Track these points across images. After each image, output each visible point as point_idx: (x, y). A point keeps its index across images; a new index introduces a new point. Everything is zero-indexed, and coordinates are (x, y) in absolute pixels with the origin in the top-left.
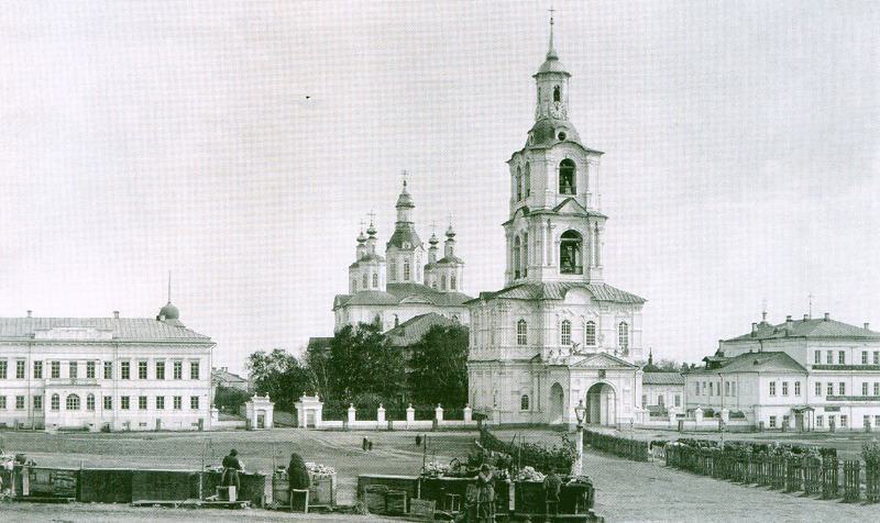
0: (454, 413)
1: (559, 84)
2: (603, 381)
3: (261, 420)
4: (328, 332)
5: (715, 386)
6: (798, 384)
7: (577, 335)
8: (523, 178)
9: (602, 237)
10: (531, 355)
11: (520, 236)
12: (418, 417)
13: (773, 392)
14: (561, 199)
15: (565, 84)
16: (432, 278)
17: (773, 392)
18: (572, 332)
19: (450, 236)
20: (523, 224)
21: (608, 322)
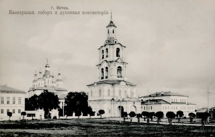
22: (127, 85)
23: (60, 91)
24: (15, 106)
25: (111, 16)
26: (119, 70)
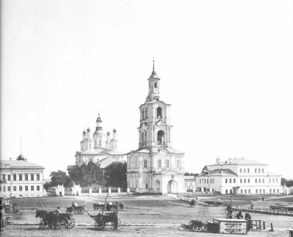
0: (124, 190)
1: (156, 82)
2: (173, 179)
3: (61, 193)
4: (73, 163)
5: (206, 180)
6: (234, 180)
7: (163, 165)
8: (145, 113)
9: (171, 132)
10: (149, 170)
11: (144, 132)
12: (103, 192)
13: (226, 182)
14: (157, 120)
15: (158, 82)
16: (108, 145)
17: (226, 182)
18: (162, 163)
19: (115, 131)
20: (144, 128)
21: (173, 160)
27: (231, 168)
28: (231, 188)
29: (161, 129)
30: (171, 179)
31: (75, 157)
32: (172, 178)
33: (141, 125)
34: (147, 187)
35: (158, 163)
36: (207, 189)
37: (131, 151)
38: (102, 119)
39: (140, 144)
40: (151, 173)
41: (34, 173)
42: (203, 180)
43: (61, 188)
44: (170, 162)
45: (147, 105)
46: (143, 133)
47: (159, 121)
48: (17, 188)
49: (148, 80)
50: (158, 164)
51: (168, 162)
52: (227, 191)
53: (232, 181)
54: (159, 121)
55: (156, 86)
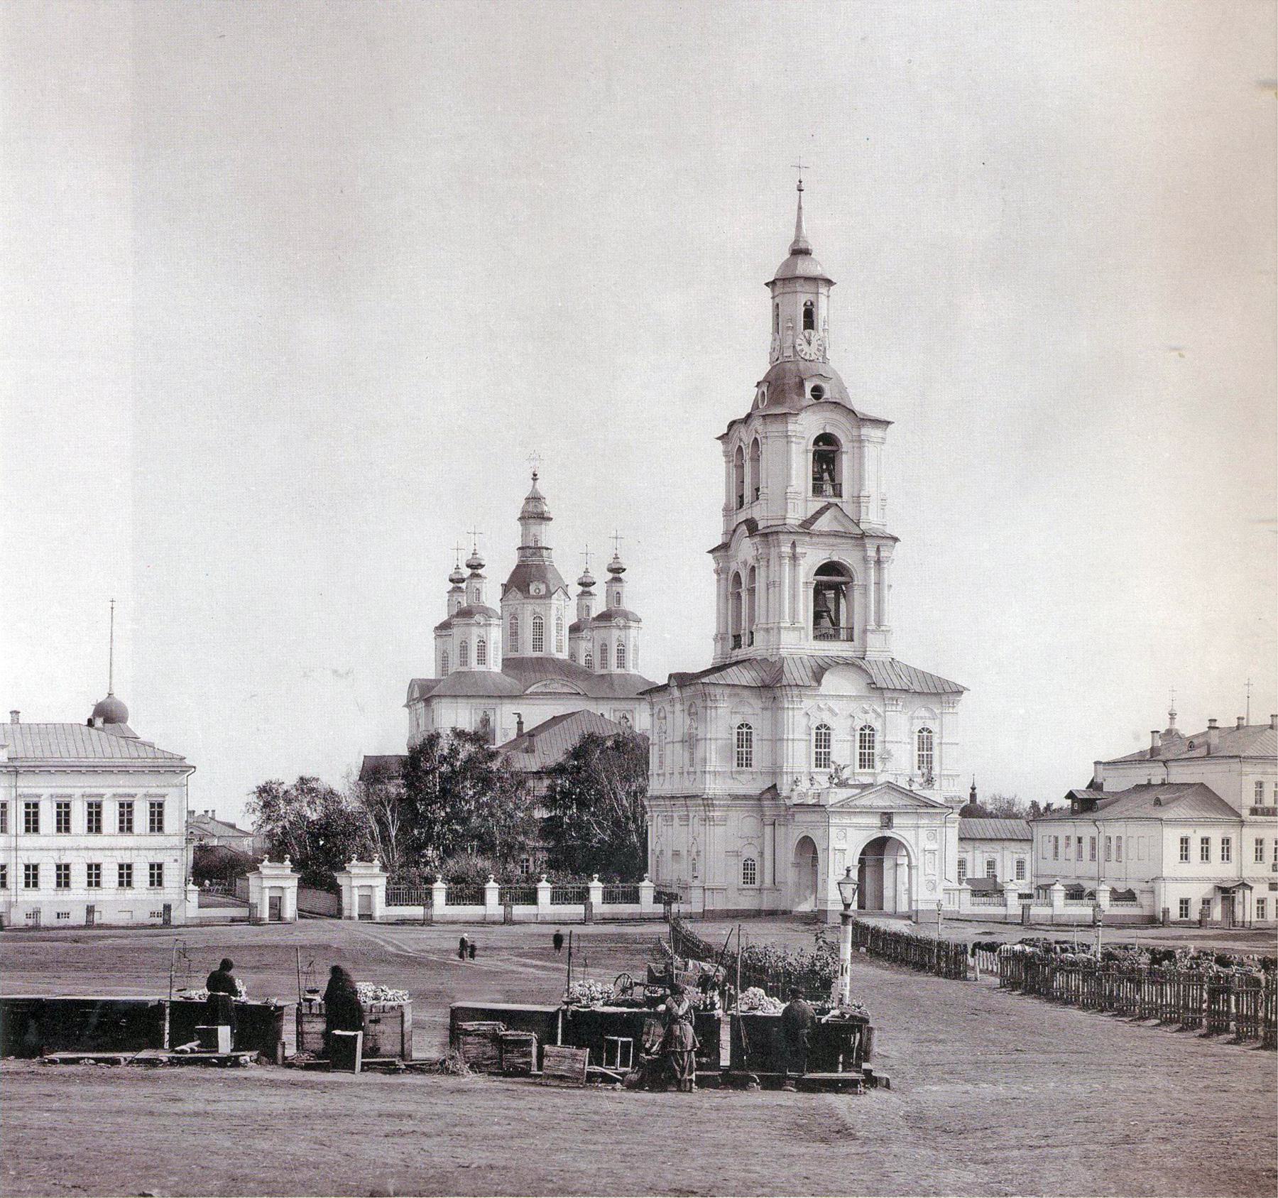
2: (888, 833)
3: (276, 905)
6: (1226, 841)
10: (755, 788)
16: (584, 647)
20: (746, 549)
21: (899, 728)
22: (878, 693)
23: (114, 659)
24: (44, 845)
25: (800, 208)
26: (830, 586)
27: (1212, 775)
28: (1205, 890)
29: (835, 559)
30: (877, 834)
31: (407, 710)
32: (882, 827)
33: (732, 533)
34: (749, 877)
35: (858, 744)
36: (1087, 891)
37: (670, 676)
38: (548, 508)
39: (720, 638)
40: (770, 802)
41: (102, 796)
42: (1068, 845)
43: (277, 877)
44: (878, 738)
45: (757, 423)
46: (737, 575)
47: (820, 513)
48: (104, 872)
49: (768, 290)
50: (814, 750)
51: (866, 738)
52: (1184, 903)
53: (1216, 849)
54: (820, 513)
55: (809, 319)
